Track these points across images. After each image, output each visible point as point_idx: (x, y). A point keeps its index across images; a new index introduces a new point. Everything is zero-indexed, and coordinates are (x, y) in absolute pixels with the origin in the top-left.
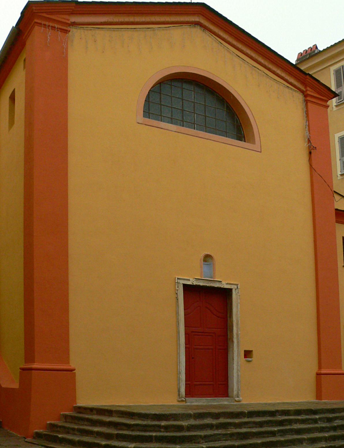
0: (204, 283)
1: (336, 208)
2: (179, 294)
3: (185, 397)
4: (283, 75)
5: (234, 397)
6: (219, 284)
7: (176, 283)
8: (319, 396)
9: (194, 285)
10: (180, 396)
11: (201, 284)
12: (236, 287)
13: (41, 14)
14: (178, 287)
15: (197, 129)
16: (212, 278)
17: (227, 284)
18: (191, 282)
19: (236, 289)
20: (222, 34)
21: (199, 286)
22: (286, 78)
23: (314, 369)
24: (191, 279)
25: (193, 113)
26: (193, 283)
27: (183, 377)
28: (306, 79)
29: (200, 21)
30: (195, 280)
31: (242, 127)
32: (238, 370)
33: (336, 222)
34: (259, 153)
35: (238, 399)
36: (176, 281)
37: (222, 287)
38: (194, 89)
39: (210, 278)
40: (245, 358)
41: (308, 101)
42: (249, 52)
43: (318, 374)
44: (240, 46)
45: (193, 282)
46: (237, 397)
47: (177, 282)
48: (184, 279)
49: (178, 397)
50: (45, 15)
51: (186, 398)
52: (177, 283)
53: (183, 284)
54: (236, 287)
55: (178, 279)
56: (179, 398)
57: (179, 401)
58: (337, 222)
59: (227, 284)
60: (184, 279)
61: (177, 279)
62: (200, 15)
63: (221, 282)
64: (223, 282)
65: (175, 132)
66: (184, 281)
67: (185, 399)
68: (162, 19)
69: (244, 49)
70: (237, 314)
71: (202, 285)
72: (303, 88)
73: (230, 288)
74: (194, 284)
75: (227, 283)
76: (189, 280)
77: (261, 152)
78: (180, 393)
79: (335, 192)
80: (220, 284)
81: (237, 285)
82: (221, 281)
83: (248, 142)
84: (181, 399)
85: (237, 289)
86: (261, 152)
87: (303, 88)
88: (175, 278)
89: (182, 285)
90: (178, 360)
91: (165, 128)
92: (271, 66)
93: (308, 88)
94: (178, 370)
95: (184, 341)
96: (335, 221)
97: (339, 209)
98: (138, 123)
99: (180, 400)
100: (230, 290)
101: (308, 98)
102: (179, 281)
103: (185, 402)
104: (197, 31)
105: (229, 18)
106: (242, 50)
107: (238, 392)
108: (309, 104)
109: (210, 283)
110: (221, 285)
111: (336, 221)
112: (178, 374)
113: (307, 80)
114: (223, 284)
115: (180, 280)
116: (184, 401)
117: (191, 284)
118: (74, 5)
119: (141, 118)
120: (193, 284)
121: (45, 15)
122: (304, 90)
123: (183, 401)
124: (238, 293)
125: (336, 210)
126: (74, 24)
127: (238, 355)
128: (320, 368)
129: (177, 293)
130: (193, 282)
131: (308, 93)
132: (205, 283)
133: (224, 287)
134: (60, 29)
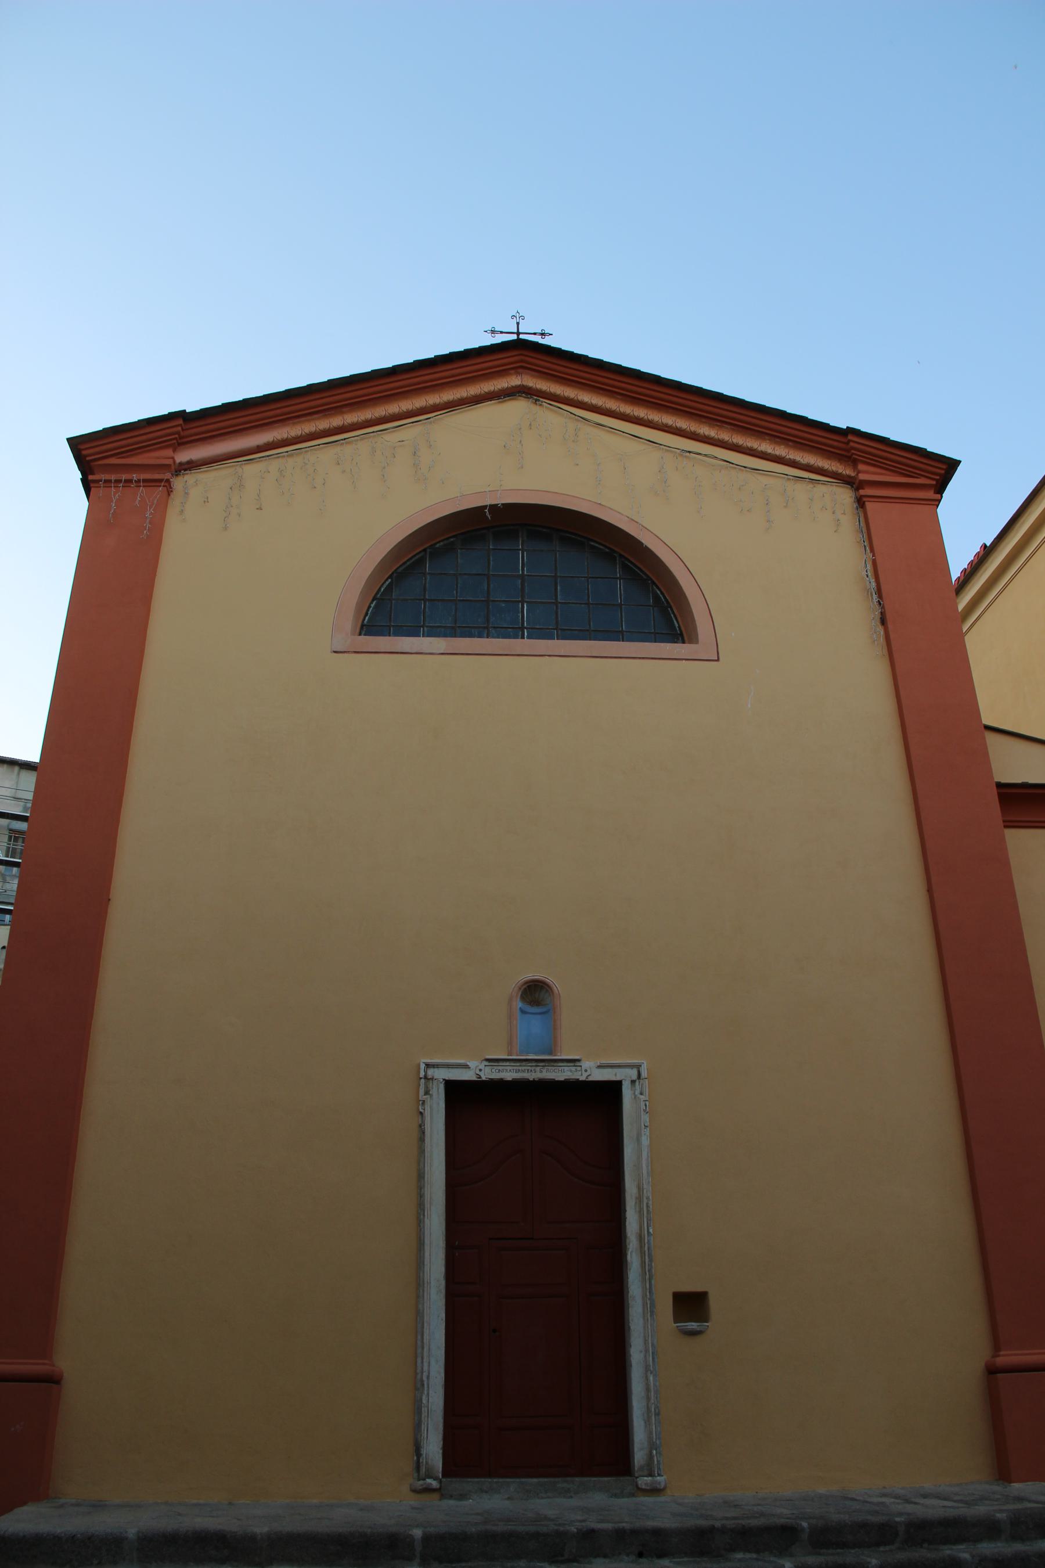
0: (517, 1071)
1: (997, 780)
2: (427, 1114)
3: (445, 1474)
6: (571, 1071)
7: (421, 1078)
9: (483, 1081)
10: (423, 1470)
11: (509, 1074)
13: (100, 462)
14: (427, 1093)
15: (528, 638)
16: (551, 1054)
17: (599, 1067)
18: (476, 1070)
19: (633, 1082)
20: (586, 397)
21: (501, 1083)
22: (788, 457)
24: (472, 1064)
25: (422, 600)
26: (482, 1074)
27: (435, 1398)
30: (487, 1063)
31: (672, 610)
32: (647, 1368)
33: (1006, 827)
34: (716, 663)
36: (422, 1074)
37: (582, 1078)
39: (543, 1053)
43: (992, 1371)
44: (641, 412)
46: (646, 1473)
47: (425, 1077)
48: (448, 1066)
49: (416, 1475)
50: (114, 461)
52: (423, 1081)
53: (444, 1080)
55: (428, 1066)
57: (414, 1491)
58: (1009, 824)
60: (448, 1066)
61: (423, 1066)
62: (520, 370)
63: (578, 1064)
64: (586, 1064)
66: (450, 1070)
67: (441, 1482)
68: (419, 402)
69: (655, 416)
70: (638, 1166)
71: (510, 1079)
75: (599, 1064)
76: (466, 1067)
77: (718, 660)
78: (423, 1460)
80: (576, 1070)
81: (638, 1067)
82: (579, 1060)
83: (690, 642)
84: (421, 1482)
85: (637, 1083)
86: (718, 660)
88: (419, 1065)
90: (419, 1337)
93: (861, 467)
94: (416, 1374)
95: (443, 1269)
96: (1002, 824)
97: (1003, 781)
100: (613, 1089)
101: (862, 492)
102: (431, 1072)
103: (435, 1496)
104: (519, 407)
105: (591, 355)
107: (650, 1457)
108: (869, 506)
109: (538, 1069)
111: (1004, 821)
113: (852, 444)
115: (436, 1070)
117: (474, 1078)
118: (181, 422)
120: (480, 1077)
121: (114, 461)
122: (853, 474)
123: (428, 1490)
124: (641, 1094)
125: (999, 785)
126: (191, 466)
127: (650, 1308)
128: (997, 1345)
129: (421, 1110)
130: (480, 1070)
132: (524, 1071)
133: (590, 1079)
134: (145, 481)
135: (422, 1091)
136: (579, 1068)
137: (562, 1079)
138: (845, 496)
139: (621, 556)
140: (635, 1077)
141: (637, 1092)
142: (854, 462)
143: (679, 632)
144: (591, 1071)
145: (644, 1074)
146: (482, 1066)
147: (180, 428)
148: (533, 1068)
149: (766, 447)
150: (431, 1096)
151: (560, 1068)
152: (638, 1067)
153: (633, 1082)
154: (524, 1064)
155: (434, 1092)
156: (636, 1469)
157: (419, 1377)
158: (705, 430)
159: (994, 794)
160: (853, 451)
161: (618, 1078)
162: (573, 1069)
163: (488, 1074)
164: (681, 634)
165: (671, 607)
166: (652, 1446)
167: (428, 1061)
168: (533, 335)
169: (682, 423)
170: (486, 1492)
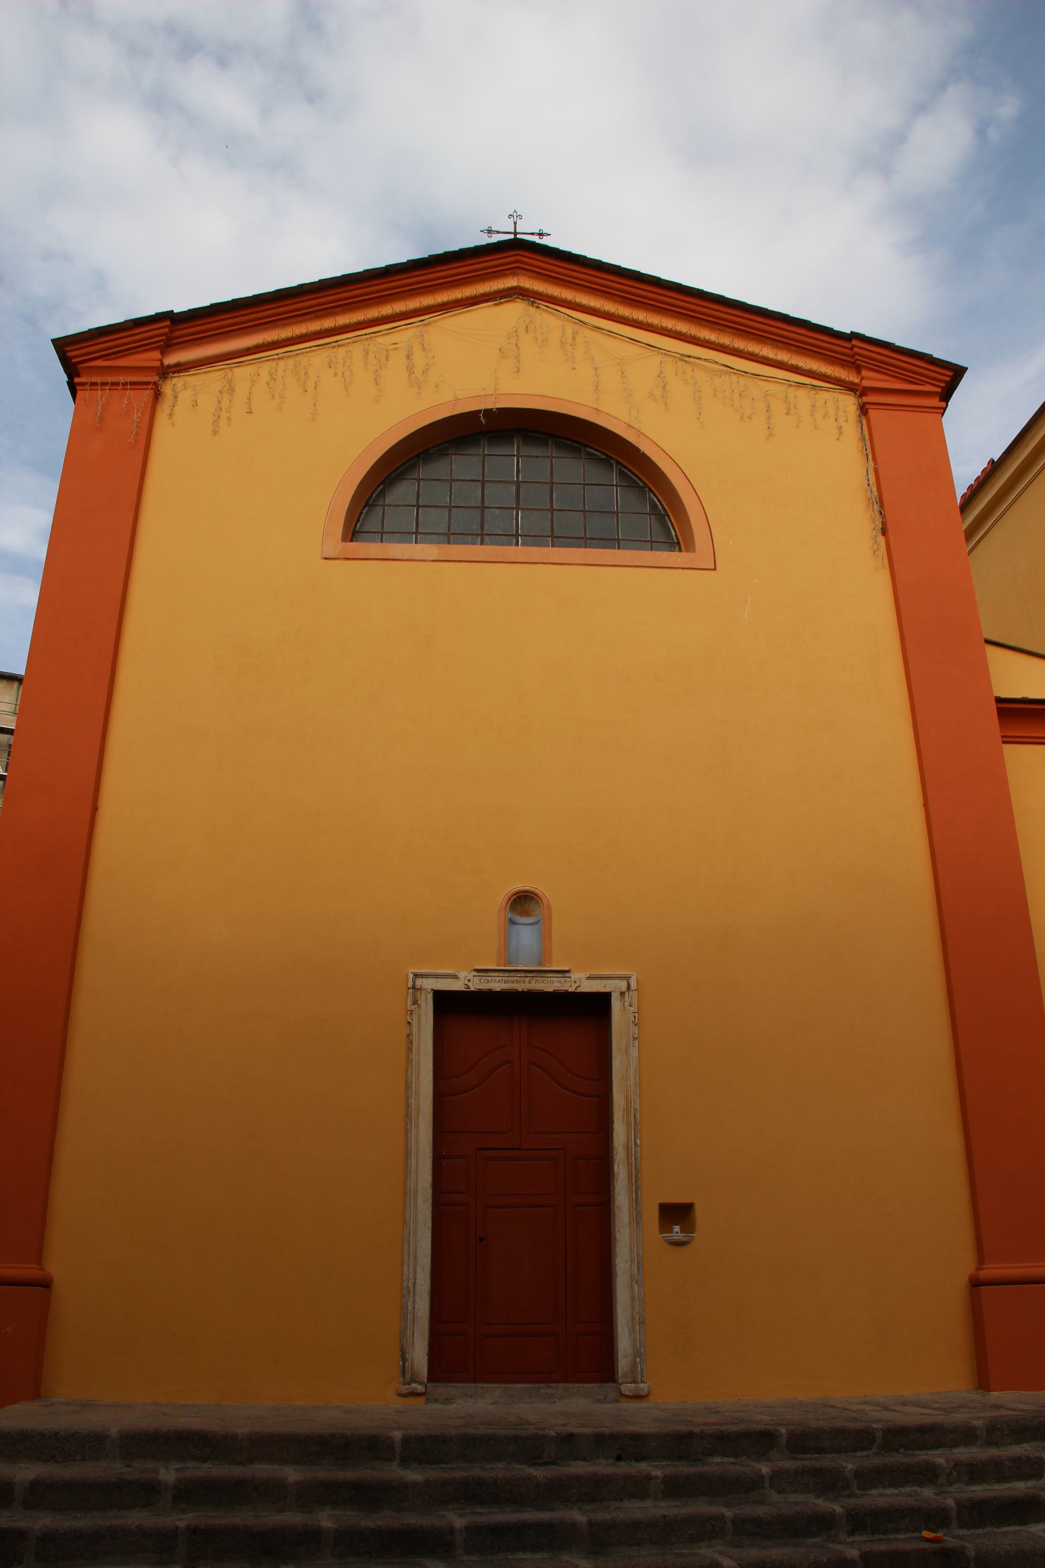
0: (506, 982)
1: (995, 695)
4: (783, 356)
5: (620, 1382)
6: (560, 982)
8: (983, 1382)
10: (408, 1375)
11: (497, 985)
12: (623, 985)
14: (415, 1002)
16: (540, 964)
17: (589, 978)
18: (464, 981)
19: (622, 994)
22: (790, 362)
23: (965, 1265)
24: (462, 974)
26: (470, 984)
28: (851, 349)
29: (522, 285)
30: (476, 974)
31: (669, 518)
35: (630, 1391)
36: (410, 984)
37: (572, 989)
38: (518, 451)
40: (661, 1232)
41: (867, 406)
42: (668, 323)
43: (975, 1283)
44: (640, 315)
45: (469, 980)
46: (629, 1380)
51: (428, 1384)
53: (432, 990)
54: (623, 985)
56: (405, 1384)
59: (589, 978)
63: (567, 975)
65: (435, 561)
69: (654, 319)
71: (498, 989)
72: (852, 378)
73: (603, 990)
74: (472, 989)
75: (588, 975)
76: (455, 977)
77: (715, 569)
79: (988, 642)
81: (627, 978)
82: (568, 971)
86: (715, 569)
87: (852, 378)
89: (430, 996)
91: (404, 558)
92: (740, 344)
93: (864, 373)
94: (403, 1281)
95: (430, 1178)
98: (326, 559)
99: (404, 1389)
102: (419, 982)
104: (515, 310)
106: (764, 357)
110: (569, 984)
111: (1003, 737)
112: (403, 1296)
114: (573, 979)
115: (424, 979)
116: (419, 1395)
117: (463, 988)
118: (168, 323)
119: (335, 544)
123: (414, 1394)
124: (631, 1006)
125: (999, 700)
126: (181, 368)
128: (981, 1260)
129: (410, 1021)
130: (469, 980)
131: (866, 383)
132: (512, 982)
133: (579, 990)
134: (132, 383)
135: (409, 1002)
136: (568, 979)
137: (551, 990)
138: (849, 403)
139: (618, 463)
140: (624, 989)
141: (627, 1004)
142: (858, 369)
143: (676, 541)
144: (581, 982)
145: (633, 986)
146: (470, 977)
147: (167, 330)
148: (522, 979)
149: (767, 352)
150: (419, 1006)
151: (549, 979)
152: (627, 978)
153: (622, 994)
154: (513, 974)
155: (422, 1002)
156: (620, 1376)
157: (405, 1284)
158: (705, 334)
159: (993, 706)
160: (856, 357)
161: (607, 990)
162: (563, 980)
163: (477, 984)
164: (678, 543)
165: (668, 515)
166: (637, 1353)
167: (417, 971)
168: (501, 231)
169: (682, 327)
170: (471, 1397)
